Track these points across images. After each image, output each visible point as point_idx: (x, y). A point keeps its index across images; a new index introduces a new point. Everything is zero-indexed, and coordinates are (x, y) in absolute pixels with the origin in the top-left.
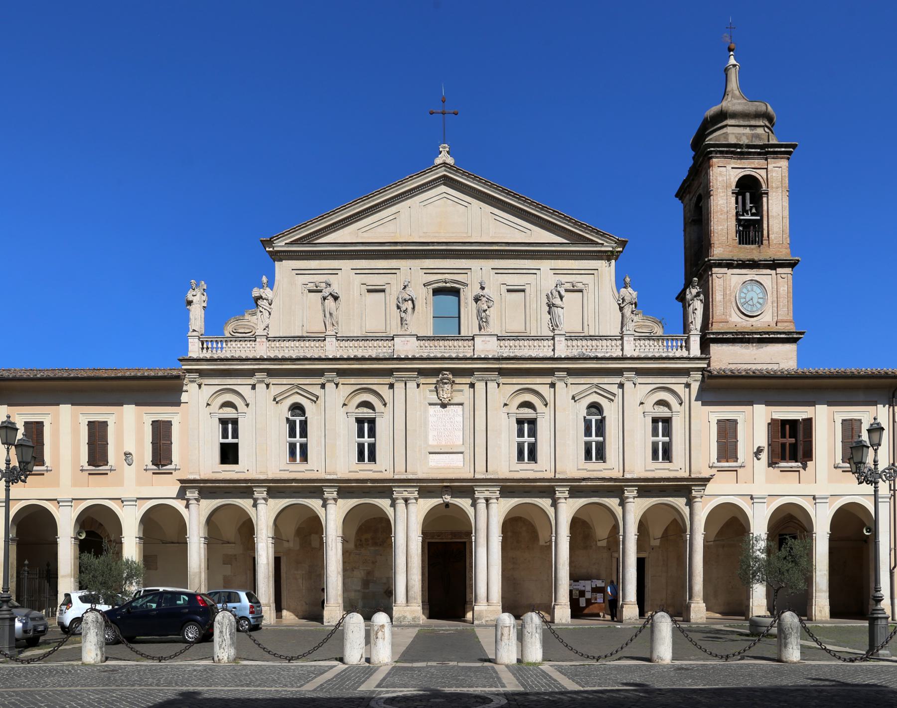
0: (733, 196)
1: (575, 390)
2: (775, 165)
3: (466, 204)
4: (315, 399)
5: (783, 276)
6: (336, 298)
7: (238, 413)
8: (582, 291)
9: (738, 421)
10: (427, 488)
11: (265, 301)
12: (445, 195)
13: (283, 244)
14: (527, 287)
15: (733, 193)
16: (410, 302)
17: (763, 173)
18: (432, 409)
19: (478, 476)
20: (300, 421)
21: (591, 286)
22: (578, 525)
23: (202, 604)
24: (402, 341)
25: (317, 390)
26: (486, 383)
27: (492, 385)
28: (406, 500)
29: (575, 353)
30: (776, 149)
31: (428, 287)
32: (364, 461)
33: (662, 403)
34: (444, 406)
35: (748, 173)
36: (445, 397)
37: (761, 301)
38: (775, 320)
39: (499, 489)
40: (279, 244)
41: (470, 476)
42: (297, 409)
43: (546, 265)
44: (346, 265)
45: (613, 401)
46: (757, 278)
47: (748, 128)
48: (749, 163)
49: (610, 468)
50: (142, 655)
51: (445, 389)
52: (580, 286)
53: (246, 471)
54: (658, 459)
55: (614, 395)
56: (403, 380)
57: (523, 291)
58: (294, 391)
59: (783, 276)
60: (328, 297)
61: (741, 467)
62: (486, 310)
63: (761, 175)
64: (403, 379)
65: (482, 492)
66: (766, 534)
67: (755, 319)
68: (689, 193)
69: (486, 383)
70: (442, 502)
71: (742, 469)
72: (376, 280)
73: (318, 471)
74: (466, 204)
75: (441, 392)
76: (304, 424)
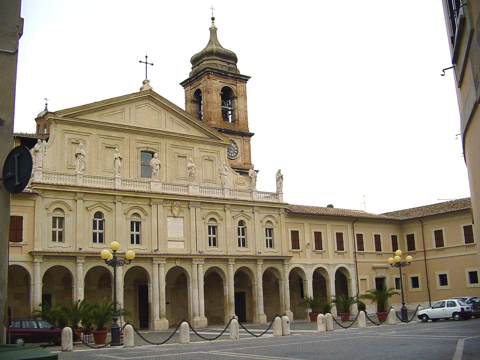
0: (220, 96)
1: (234, 214)
2: (241, 85)
3: (158, 111)
4: (110, 210)
5: (246, 141)
6: (121, 159)
7: (65, 215)
8: (212, 161)
9: (23, 217)
10: (170, 258)
11: (82, 156)
12: (148, 104)
13: (61, 116)
14: (188, 156)
15: (220, 94)
16: (159, 166)
17: (234, 87)
18: (169, 219)
19: (193, 253)
20: (99, 221)
21: (217, 158)
22: (48, 277)
23: (83, 324)
24: (155, 184)
25: (111, 206)
26: (195, 208)
27: (198, 210)
28: (159, 264)
29: (233, 197)
30: (241, 77)
31: (139, 149)
32: (134, 244)
33: (212, 219)
34: (174, 217)
35: (227, 86)
36: (176, 213)
37: (236, 152)
38: (243, 163)
39: (204, 260)
40: (58, 116)
41: (188, 253)
42: (99, 215)
43: (196, 146)
44: (95, 132)
45: (249, 220)
46: (233, 139)
47: (226, 63)
48: (228, 81)
49: (249, 251)
50: (150, 343)
51: (176, 210)
52: (212, 158)
53: (69, 247)
54: (240, 246)
55: (250, 217)
56: (156, 204)
57: (186, 157)
58: (98, 205)
59: (246, 141)
60: (118, 158)
61: (301, 251)
62: (195, 174)
63: (233, 87)
64: (156, 203)
65: (196, 261)
66: (123, 284)
67: (233, 161)
68: (190, 85)
69: (195, 208)
70: (175, 266)
71: (302, 252)
72: (111, 143)
73: (70, 247)
74: (158, 111)
75: (174, 211)
76: (101, 223)
